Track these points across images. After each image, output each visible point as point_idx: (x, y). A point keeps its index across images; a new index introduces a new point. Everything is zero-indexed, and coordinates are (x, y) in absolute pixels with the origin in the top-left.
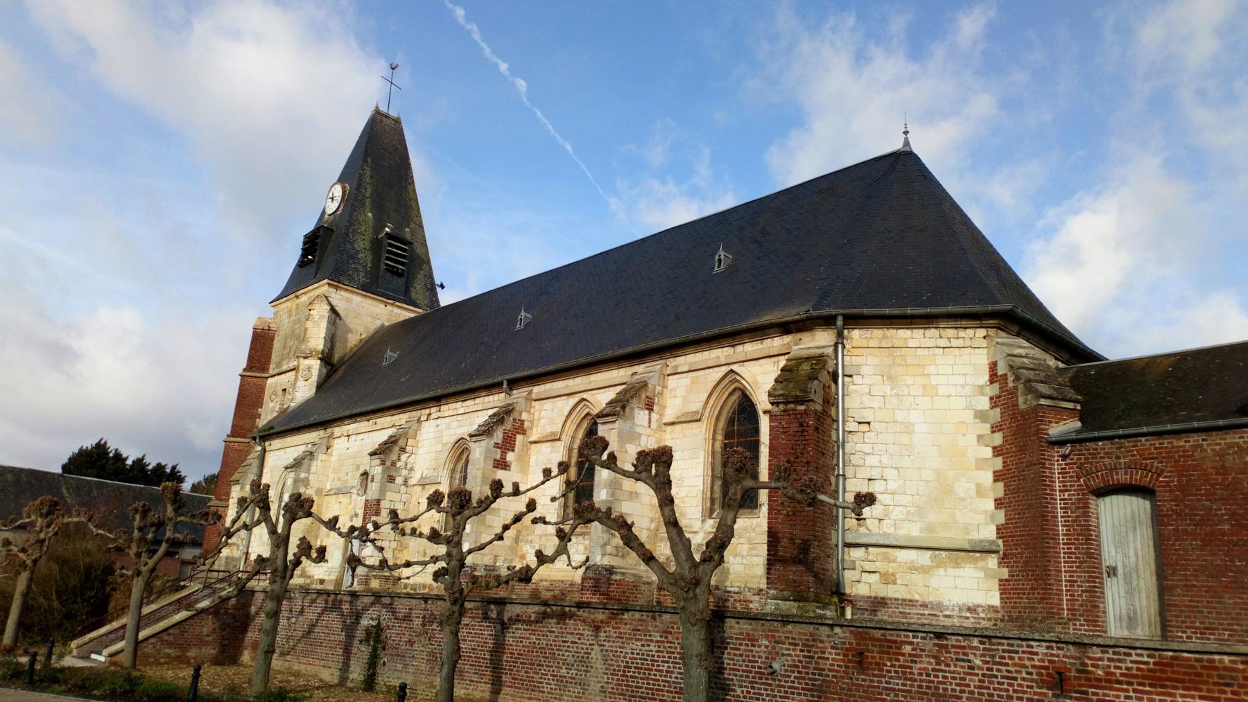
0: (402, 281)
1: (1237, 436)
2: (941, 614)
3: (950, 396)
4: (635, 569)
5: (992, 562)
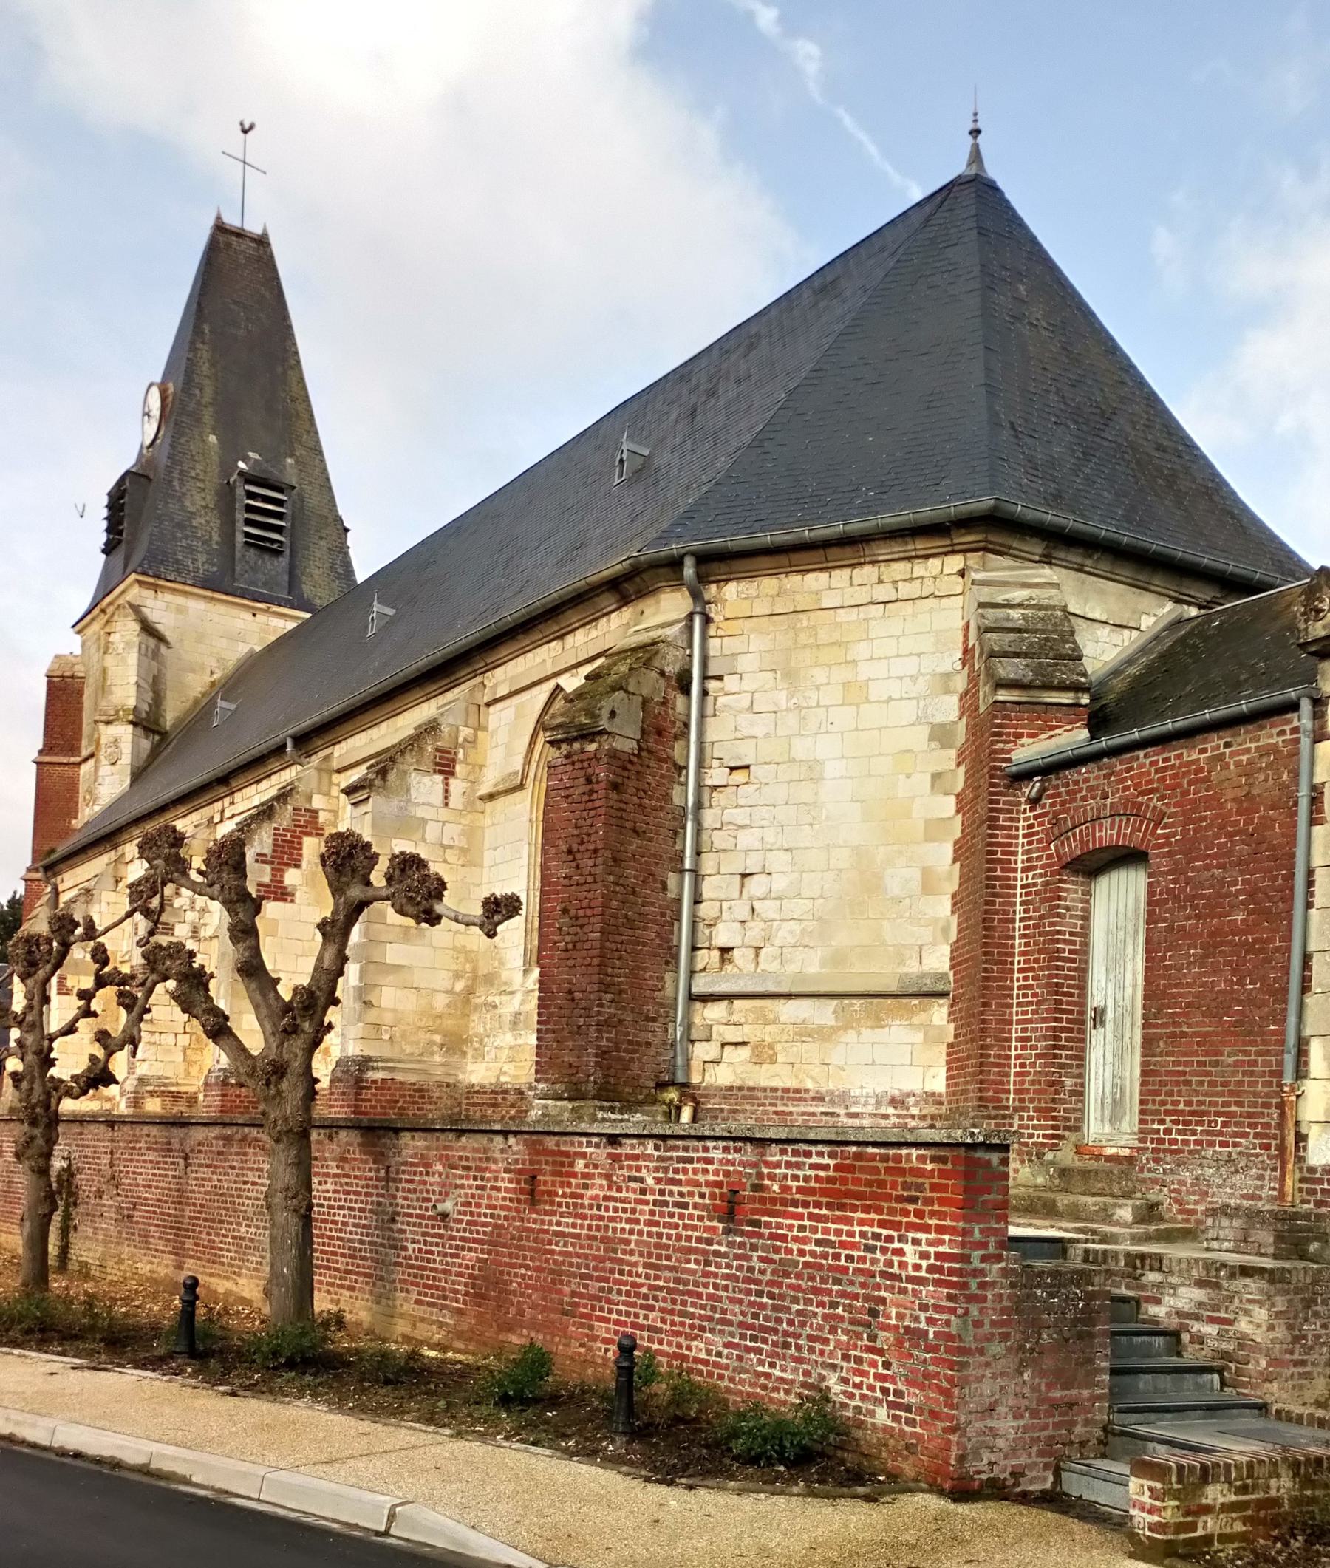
0: (284, 561)
1: (1275, 731)
2: (842, 1111)
3: (890, 699)
4: (419, 1062)
5: (939, 1012)
